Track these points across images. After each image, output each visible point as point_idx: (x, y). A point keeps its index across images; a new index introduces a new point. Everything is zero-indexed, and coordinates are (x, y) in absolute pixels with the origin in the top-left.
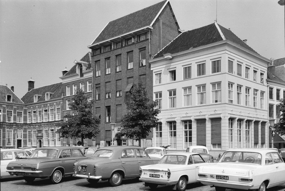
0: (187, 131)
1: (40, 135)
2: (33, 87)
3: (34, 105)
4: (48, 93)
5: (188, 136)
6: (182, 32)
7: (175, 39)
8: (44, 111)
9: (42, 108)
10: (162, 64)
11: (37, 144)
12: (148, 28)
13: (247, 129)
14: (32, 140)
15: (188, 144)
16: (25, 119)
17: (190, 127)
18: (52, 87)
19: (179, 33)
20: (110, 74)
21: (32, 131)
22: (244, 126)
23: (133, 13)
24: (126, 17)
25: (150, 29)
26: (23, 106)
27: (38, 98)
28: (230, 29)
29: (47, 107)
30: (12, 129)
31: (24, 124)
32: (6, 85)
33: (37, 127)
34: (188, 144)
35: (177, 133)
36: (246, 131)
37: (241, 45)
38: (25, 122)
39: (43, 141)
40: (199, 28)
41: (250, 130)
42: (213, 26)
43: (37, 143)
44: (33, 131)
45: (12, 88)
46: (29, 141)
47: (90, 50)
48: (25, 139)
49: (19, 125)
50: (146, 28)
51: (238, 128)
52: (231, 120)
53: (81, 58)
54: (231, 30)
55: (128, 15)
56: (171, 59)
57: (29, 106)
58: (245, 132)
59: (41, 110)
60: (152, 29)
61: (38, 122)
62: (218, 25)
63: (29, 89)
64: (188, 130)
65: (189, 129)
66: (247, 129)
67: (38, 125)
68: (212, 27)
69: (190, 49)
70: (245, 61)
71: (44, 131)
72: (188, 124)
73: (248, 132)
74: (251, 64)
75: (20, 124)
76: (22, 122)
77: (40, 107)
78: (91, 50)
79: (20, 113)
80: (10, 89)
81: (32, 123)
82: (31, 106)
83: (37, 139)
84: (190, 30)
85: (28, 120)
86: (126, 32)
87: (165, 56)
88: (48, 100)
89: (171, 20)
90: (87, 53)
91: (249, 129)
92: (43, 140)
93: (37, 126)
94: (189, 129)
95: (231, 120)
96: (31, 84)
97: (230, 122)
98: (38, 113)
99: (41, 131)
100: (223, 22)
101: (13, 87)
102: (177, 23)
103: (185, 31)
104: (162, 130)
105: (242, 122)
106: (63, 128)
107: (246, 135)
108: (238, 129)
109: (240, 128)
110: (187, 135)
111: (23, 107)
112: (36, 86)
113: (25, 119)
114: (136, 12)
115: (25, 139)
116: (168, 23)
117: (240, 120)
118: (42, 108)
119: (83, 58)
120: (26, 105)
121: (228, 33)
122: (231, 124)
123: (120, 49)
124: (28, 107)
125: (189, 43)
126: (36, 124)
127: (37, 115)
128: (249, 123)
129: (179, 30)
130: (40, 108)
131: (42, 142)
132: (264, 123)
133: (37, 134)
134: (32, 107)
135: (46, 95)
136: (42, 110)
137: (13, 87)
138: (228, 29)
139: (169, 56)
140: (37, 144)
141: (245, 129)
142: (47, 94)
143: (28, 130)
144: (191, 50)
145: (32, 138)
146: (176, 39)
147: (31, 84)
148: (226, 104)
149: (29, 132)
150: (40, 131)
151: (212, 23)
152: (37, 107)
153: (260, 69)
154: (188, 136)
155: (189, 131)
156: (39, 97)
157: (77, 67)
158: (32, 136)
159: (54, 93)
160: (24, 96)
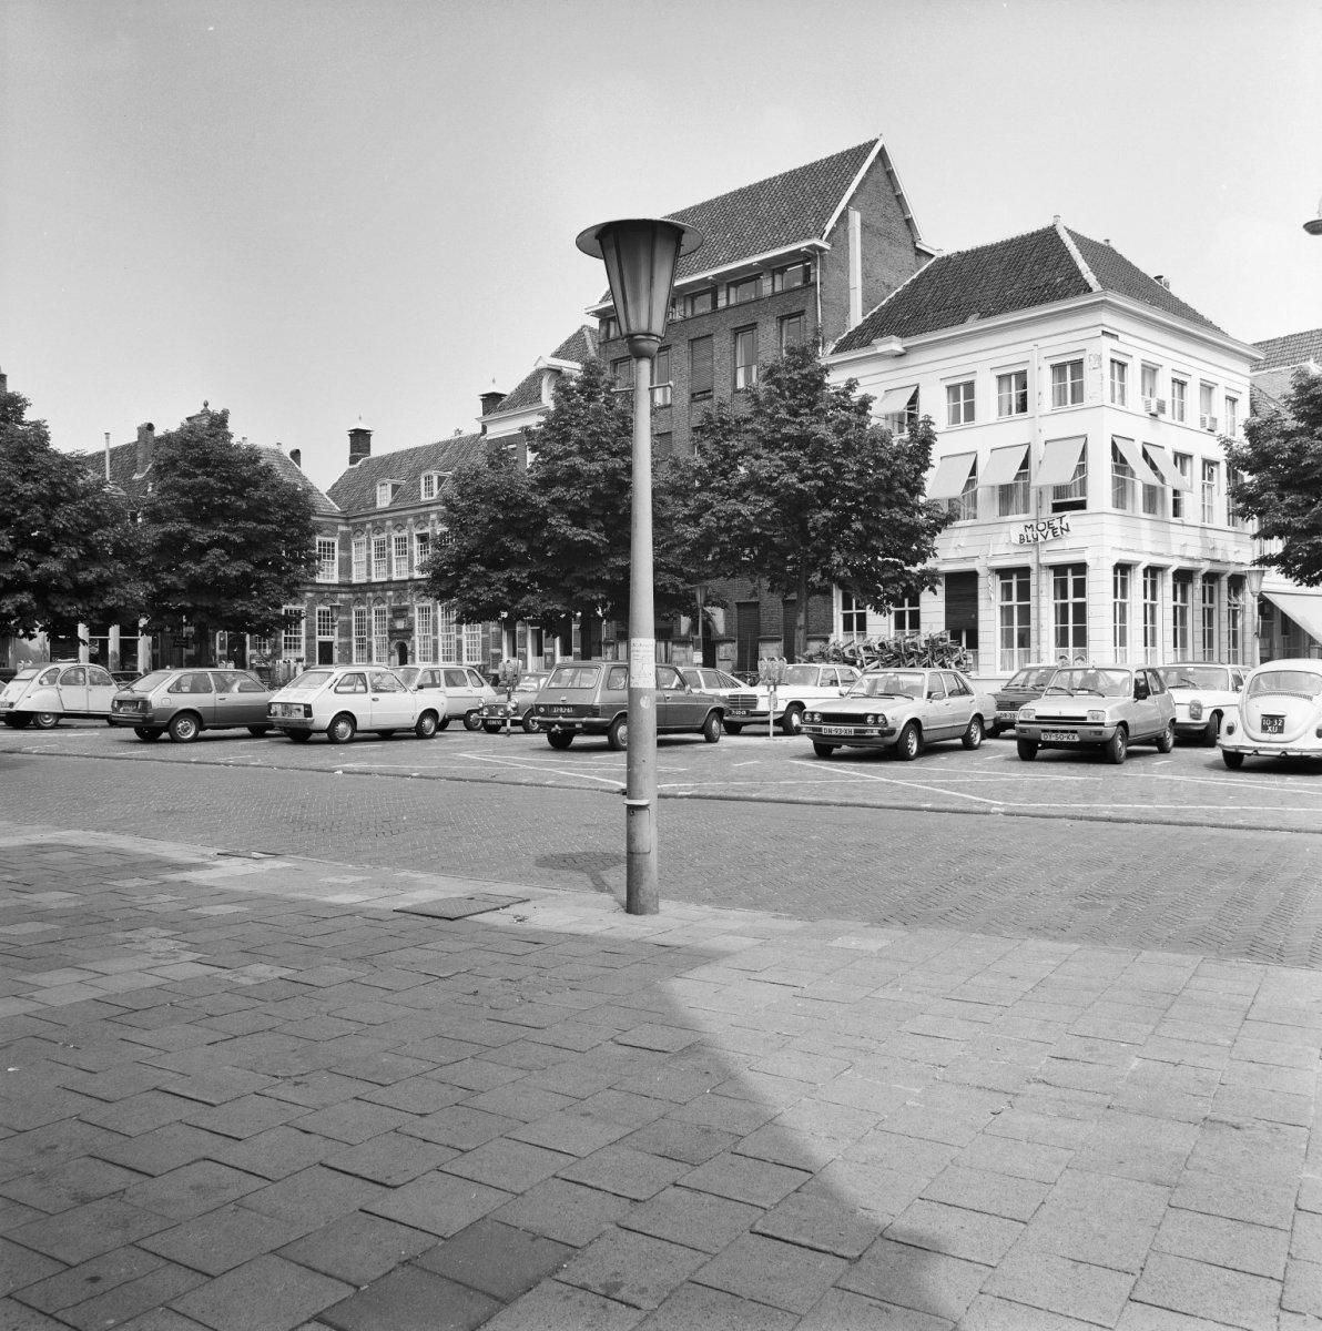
0: (1012, 607)
1: (400, 625)
2: (368, 451)
3: (378, 517)
4: (432, 473)
5: (1071, 625)
6: (938, 255)
7: (908, 282)
8: (415, 539)
9: (410, 529)
10: (874, 372)
11: (389, 659)
12: (814, 245)
13: (1179, 603)
14: (370, 643)
15: (1016, 653)
16: (346, 567)
17: (1024, 592)
18: (443, 452)
19: (916, 254)
20: (670, 405)
21: (370, 613)
22: (1199, 595)
23: (750, 187)
24: (723, 201)
25: (821, 250)
26: (336, 520)
27: (393, 492)
28: (1108, 241)
29: (430, 524)
30: (302, 602)
31: (340, 585)
32: (276, 447)
33: (390, 597)
34: (1016, 653)
35: (923, 618)
36: (1175, 608)
37: (1147, 292)
38: (345, 580)
39: (413, 648)
40: (999, 241)
41: (1190, 603)
42: (1048, 238)
43: (390, 655)
44: (374, 612)
45: (296, 454)
46: (360, 647)
47: (595, 323)
48: (343, 640)
49: (326, 589)
50: (808, 247)
51: (1145, 597)
52: (1123, 569)
53: (555, 347)
54: (1112, 244)
55: (731, 193)
56: (901, 355)
57: (361, 520)
58: (1172, 610)
59: (405, 533)
60: (828, 248)
61: (395, 578)
62: (1069, 231)
63: (353, 460)
64: (1014, 602)
65: (1018, 600)
66: (1207, 605)
67: (395, 590)
68: (1046, 242)
69: (971, 319)
70: (1173, 356)
71: (417, 610)
72: (1014, 581)
73: (1150, 613)
74: (1175, 359)
75: (329, 585)
76: (336, 580)
77: (399, 526)
78: (598, 320)
79: (324, 545)
80: (288, 455)
81: (369, 584)
82: (366, 519)
83: (391, 638)
84: (964, 250)
85: (354, 576)
86: (725, 262)
87: (880, 344)
88: (431, 498)
89: (890, 210)
90: (575, 331)
91: (1184, 599)
92: (413, 642)
93: (390, 593)
94: (1018, 600)
95: (1123, 569)
96: (360, 439)
97: (1119, 576)
98: (393, 547)
99: (406, 609)
100: (1083, 216)
101: (298, 451)
102: (909, 222)
103: (945, 254)
104: (921, 605)
105: (1159, 575)
106: (98, 582)
107: (1175, 623)
108: (1146, 601)
109: (1184, 599)
110: (1064, 619)
111: (337, 525)
112: (378, 449)
113: (346, 567)
114: (762, 185)
115: (343, 640)
116: (880, 224)
117: (1153, 571)
118: (410, 529)
119: (562, 348)
120: (348, 519)
121: (1103, 255)
122: (1152, 589)
123: (706, 320)
124: (355, 524)
125: (963, 299)
126: (386, 586)
127: (390, 555)
128: (1154, 575)
129: (918, 245)
130: (400, 527)
131: (409, 649)
132: (1237, 582)
133: (391, 620)
134: (369, 526)
135: (423, 481)
136: (411, 533)
137: (298, 451)
138: (1102, 242)
139: (895, 344)
140: (389, 659)
141: (1170, 604)
142: (429, 478)
143: (355, 609)
144: (973, 324)
145: (370, 635)
146: (913, 280)
147: (360, 439)
148: (1105, 516)
149: (359, 613)
150: (400, 613)
151: (1045, 227)
152: (389, 523)
153: (1222, 383)
154: (1071, 625)
155: (1019, 606)
156: (395, 488)
157: (545, 381)
158: (370, 629)
159: (450, 473)
160: (335, 485)
